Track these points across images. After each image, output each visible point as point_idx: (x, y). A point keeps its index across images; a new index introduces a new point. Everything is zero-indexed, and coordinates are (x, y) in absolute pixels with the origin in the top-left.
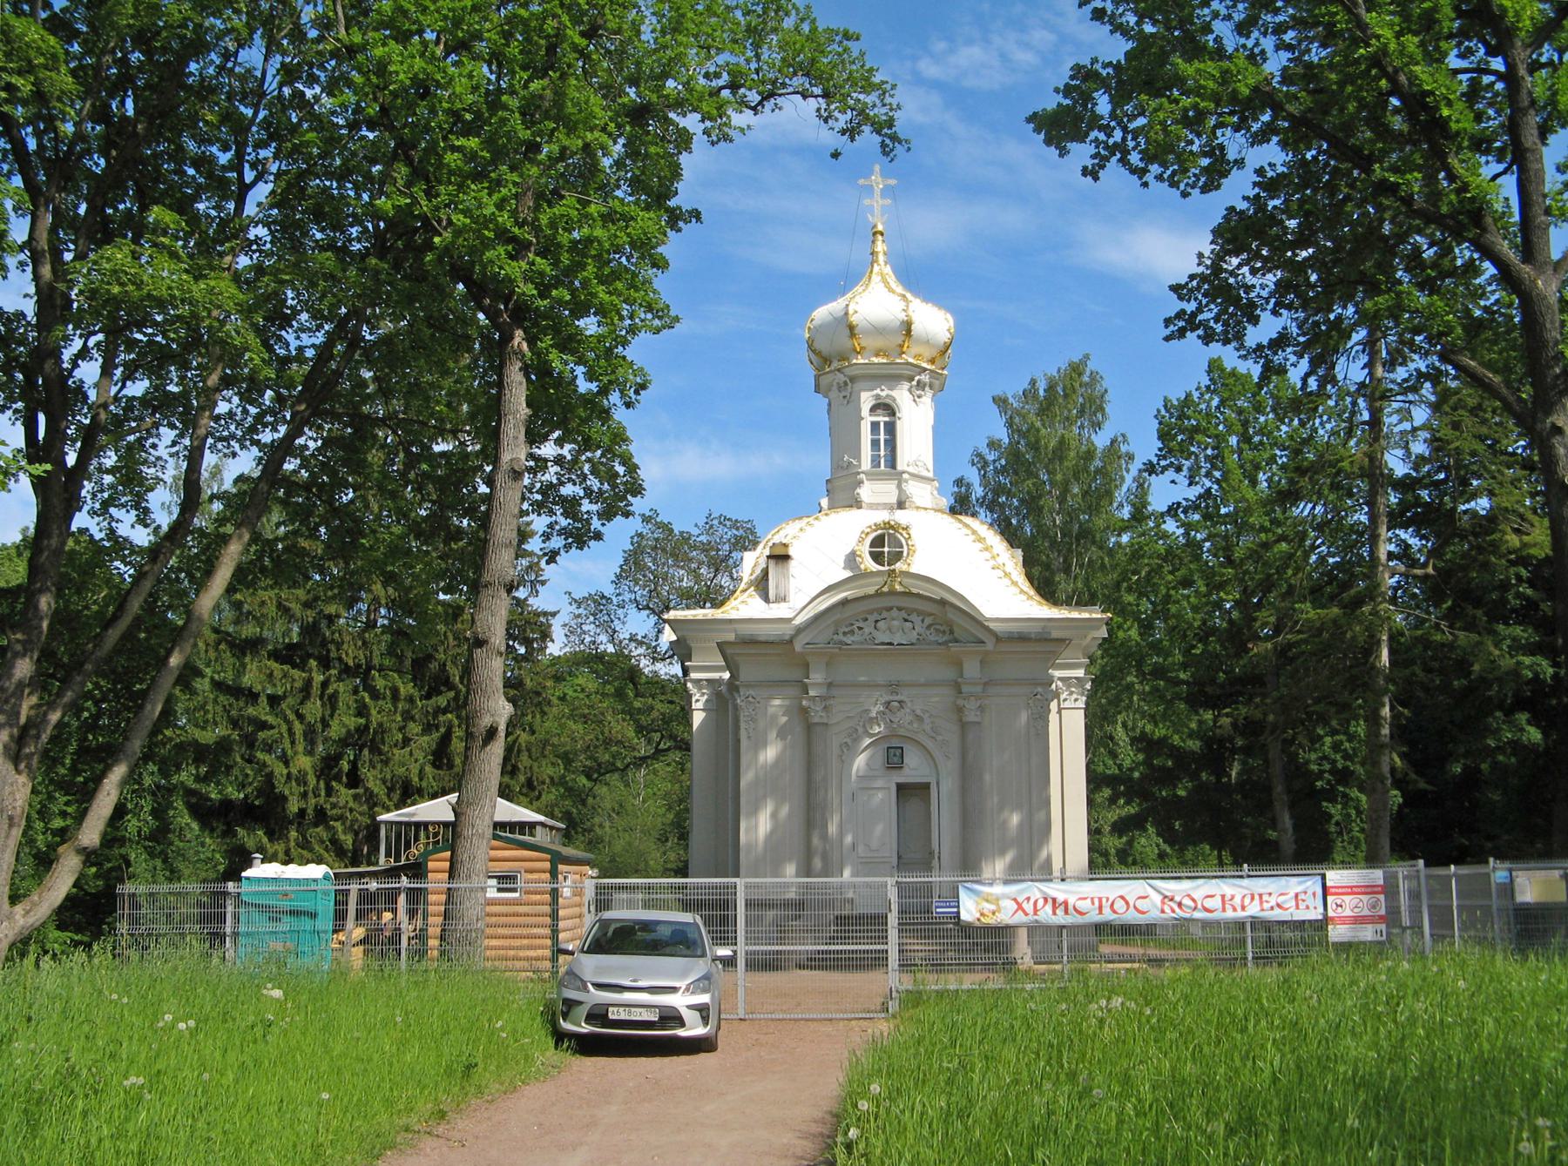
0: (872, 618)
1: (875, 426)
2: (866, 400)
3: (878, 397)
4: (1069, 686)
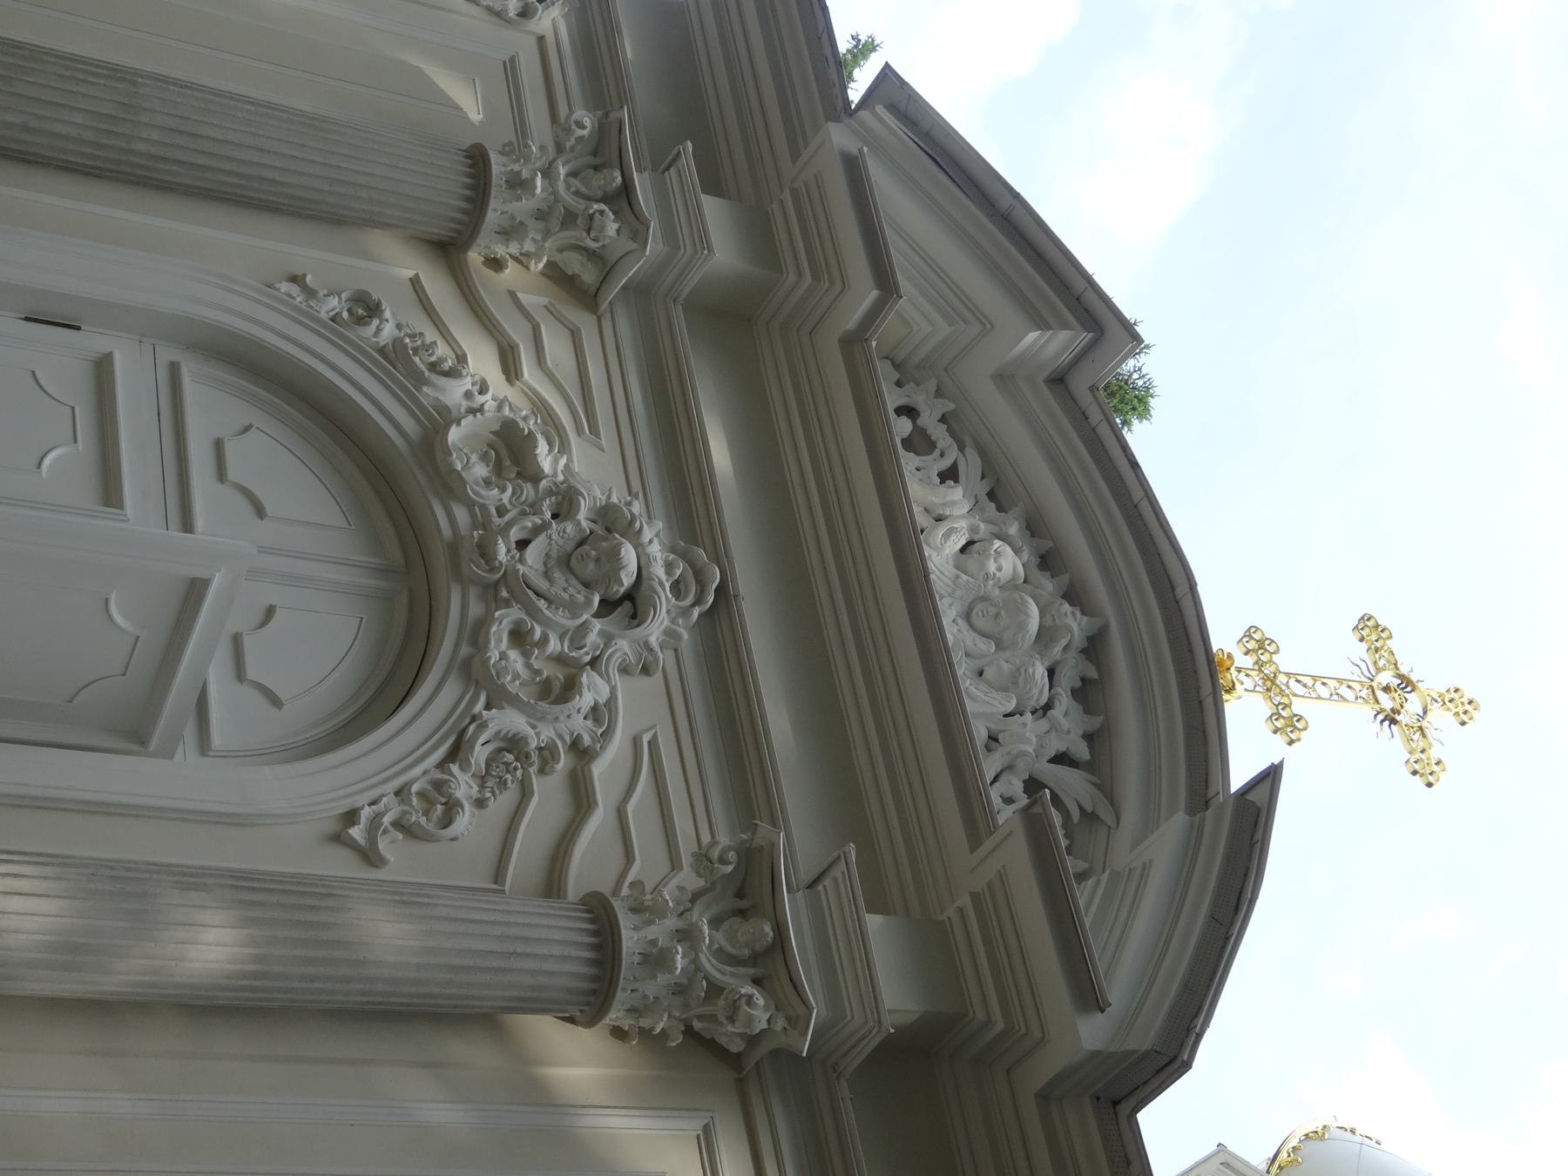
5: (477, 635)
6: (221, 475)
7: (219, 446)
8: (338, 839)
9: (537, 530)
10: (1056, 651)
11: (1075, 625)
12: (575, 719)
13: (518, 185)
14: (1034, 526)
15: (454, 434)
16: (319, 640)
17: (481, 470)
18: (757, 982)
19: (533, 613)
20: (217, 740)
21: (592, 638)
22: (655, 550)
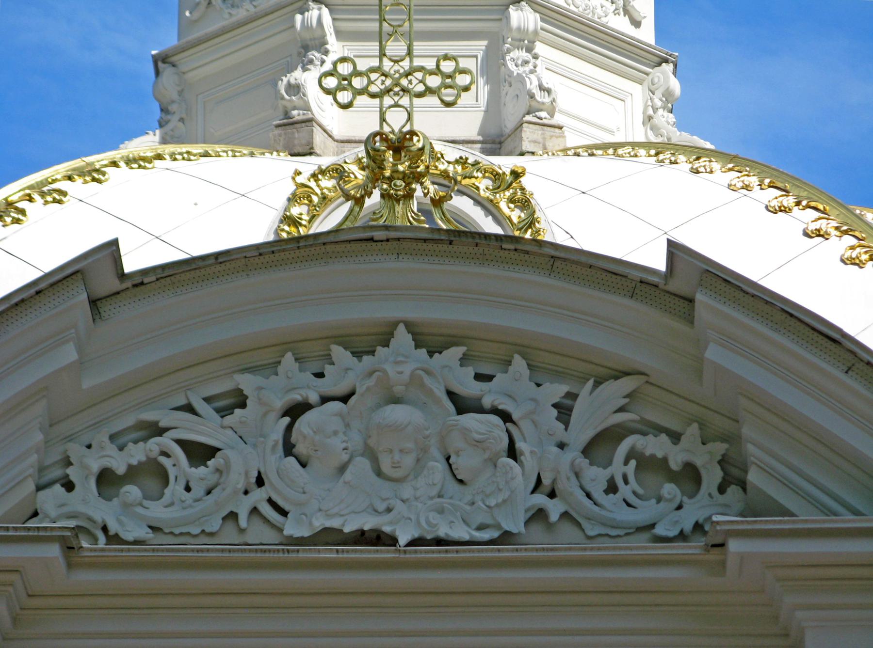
0: (268, 394)
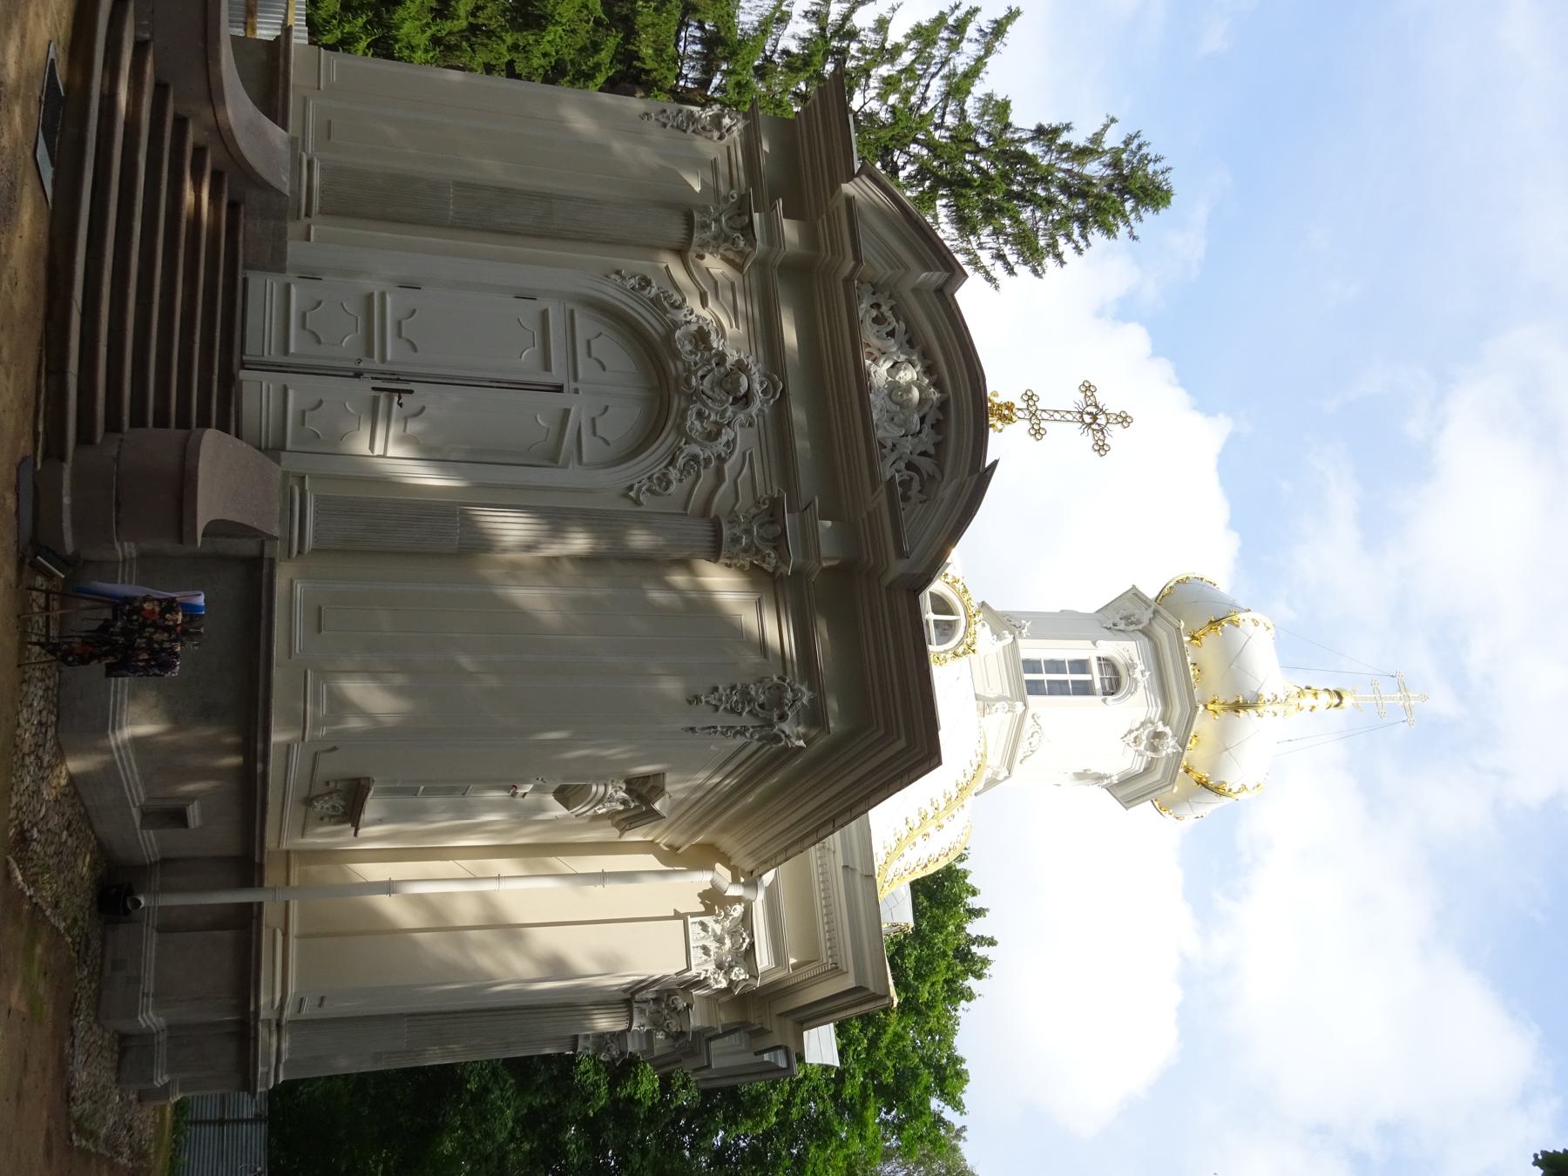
1: (1081, 666)
2: (1124, 650)
3: (1130, 667)
4: (733, 933)
5: (683, 415)
6: (589, 355)
7: (589, 342)
8: (626, 496)
9: (709, 371)
10: (926, 409)
11: (934, 395)
12: (719, 446)
13: (705, 226)
14: (926, 355)
15: (678, 333)
16: (623, 419)
17: (689, 347)
18: (775, 548)
19: (705, 405)
20: (585, 459)
21: (729, 414)
22: (756, 377)
